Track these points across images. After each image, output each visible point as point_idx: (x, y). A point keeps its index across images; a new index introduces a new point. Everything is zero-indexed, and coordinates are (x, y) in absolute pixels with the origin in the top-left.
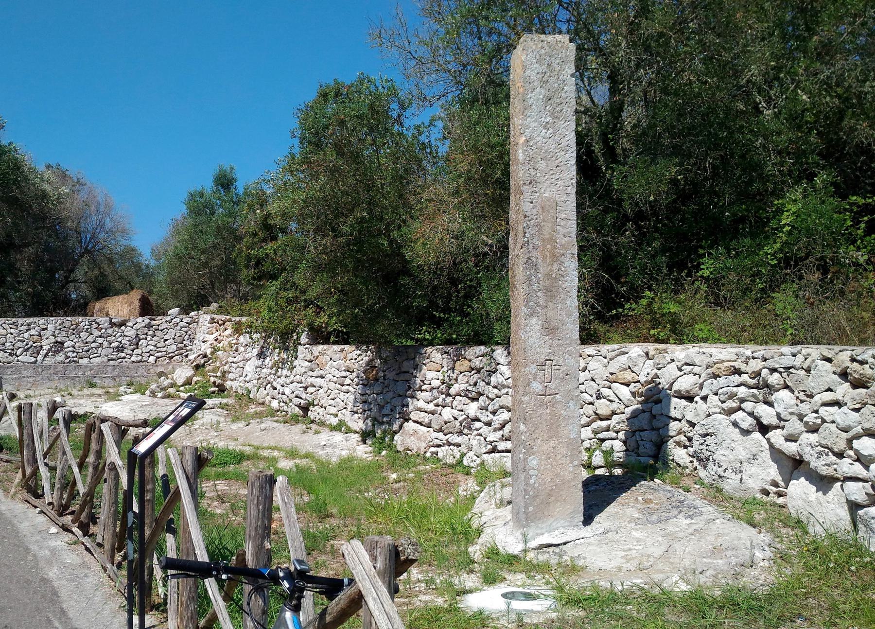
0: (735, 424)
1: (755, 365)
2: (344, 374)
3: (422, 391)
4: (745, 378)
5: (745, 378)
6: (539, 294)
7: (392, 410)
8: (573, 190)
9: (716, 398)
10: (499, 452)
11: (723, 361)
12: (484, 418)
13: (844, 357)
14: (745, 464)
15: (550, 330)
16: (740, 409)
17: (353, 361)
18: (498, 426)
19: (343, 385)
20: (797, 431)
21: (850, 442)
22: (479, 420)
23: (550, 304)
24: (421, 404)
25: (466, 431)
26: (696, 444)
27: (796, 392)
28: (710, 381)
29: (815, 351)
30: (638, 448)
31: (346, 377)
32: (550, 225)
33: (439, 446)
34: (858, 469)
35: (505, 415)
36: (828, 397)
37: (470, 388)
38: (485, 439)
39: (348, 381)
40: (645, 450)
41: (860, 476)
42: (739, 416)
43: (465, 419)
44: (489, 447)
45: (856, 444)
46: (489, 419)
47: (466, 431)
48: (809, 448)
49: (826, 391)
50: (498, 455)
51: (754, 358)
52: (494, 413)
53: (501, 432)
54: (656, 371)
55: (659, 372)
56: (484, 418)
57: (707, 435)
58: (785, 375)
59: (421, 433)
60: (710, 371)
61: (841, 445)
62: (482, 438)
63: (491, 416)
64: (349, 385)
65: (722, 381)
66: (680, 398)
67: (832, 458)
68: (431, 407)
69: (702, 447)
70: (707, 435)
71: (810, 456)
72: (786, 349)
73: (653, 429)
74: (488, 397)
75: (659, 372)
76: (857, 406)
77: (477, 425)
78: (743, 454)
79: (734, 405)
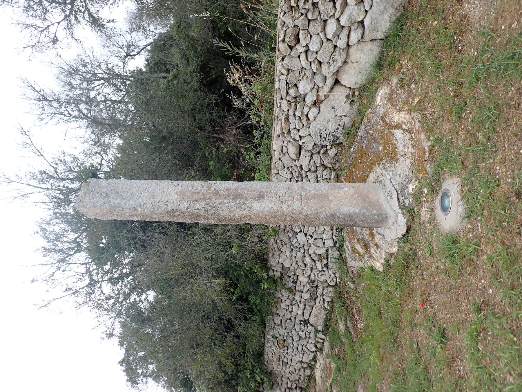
0: (315, 118)
1: (285, 106)
2: (281, 362)
3: (292, 311)
4: (291, 113)
5: (291, 113)
6: (238, 202)
7: (303, 331)
8: (176, 183)
9: (301, 131)
10: (328, 263)
11: (282, 128)
12: (309, 272)
13: (282, 47)
14: (337, 114)
15: (260, 197)
16: (307, 116)
17: (274, 356)
18: (313, 264)
19: (287, 363)
20: (321, 77)
21: (328, 40)
22: (310, 276)
23: (244, 196)
24: (300, 312)
25: (316, 284)
26: (325, 143)
27: (300, 78)
28: (292, 134)
29: (279, 68)
30: (326, 179)
31: (283, 361)
32: (195, 195)
33: (324, 300)
34: (344, 35)
35: (308, 260)
36: (303, 56)
37: (292, 280)
38: (320, 271)
39: (285, 360)
40: (328, 175)
41: (348, 33)
42: (311, 116)
43: (309, 284)
44: (325, 269)
45: (330, 36)
46: (309, 269)
47: (316, 284)
48: (331, 67)
49: (300, 58)
50: (330, 264)
51: (280, 106)
52: (306, 265)
53: (317, 262)
54: (285, 169)
55: (286, 167)
56: (309, 272)
57: (321, 136)
58: (290, 86)
59: (316, 313)
60: (286, 135)
61: (330, 45)
62: (320, 273)
63: (307, 268)
64: (287, 359)
65: (292, 126)
66: (300, 154)
67: (337, 53)
68: (302, 306)
69: (327, 139)
70: (321, 136)
71: (333, 68)
72: (276, 86)
73: (316, 171)
74: (295, 287)
75: (286, 167)
76: (309, 36)
77: (312, 276)
78: (331, 115)
79: (305, 119)
